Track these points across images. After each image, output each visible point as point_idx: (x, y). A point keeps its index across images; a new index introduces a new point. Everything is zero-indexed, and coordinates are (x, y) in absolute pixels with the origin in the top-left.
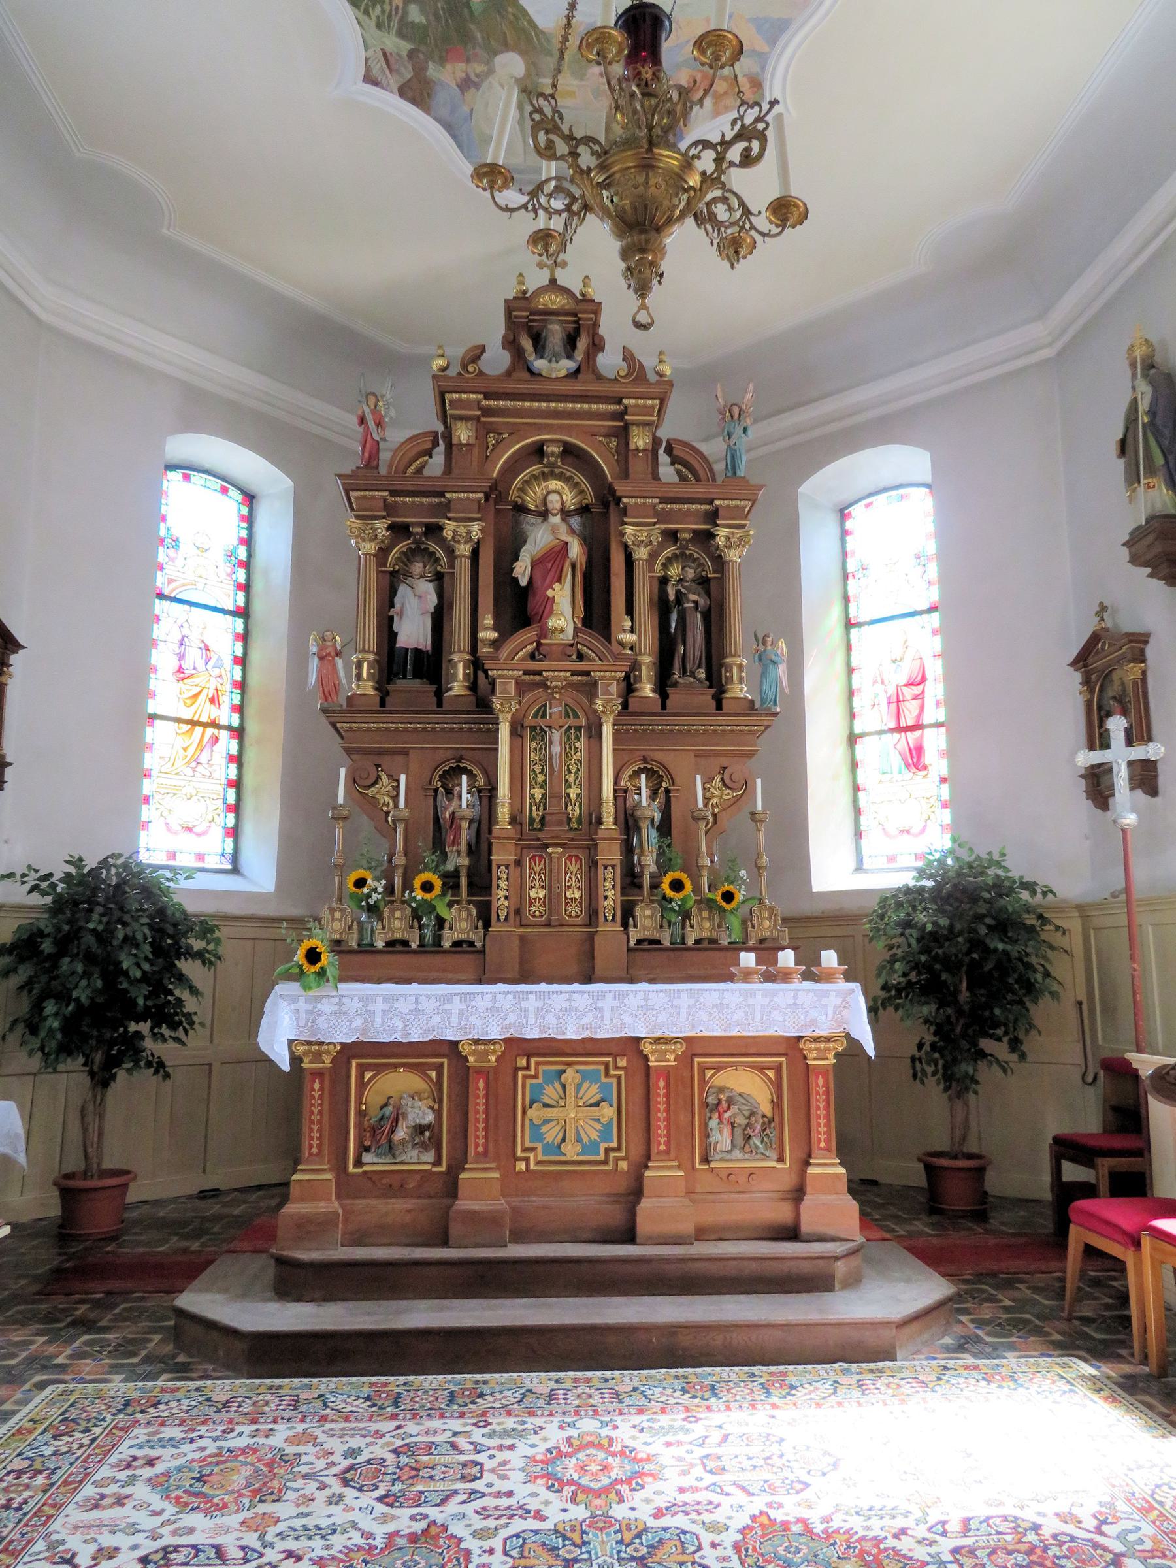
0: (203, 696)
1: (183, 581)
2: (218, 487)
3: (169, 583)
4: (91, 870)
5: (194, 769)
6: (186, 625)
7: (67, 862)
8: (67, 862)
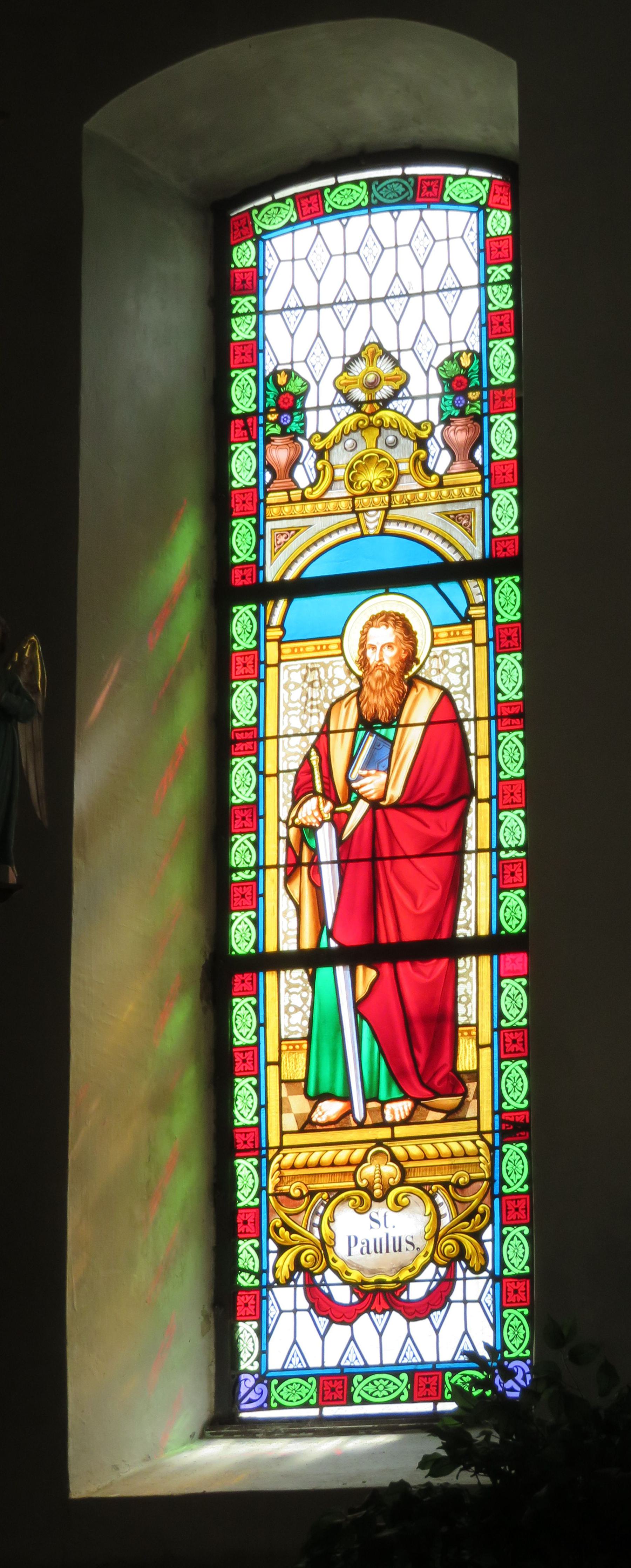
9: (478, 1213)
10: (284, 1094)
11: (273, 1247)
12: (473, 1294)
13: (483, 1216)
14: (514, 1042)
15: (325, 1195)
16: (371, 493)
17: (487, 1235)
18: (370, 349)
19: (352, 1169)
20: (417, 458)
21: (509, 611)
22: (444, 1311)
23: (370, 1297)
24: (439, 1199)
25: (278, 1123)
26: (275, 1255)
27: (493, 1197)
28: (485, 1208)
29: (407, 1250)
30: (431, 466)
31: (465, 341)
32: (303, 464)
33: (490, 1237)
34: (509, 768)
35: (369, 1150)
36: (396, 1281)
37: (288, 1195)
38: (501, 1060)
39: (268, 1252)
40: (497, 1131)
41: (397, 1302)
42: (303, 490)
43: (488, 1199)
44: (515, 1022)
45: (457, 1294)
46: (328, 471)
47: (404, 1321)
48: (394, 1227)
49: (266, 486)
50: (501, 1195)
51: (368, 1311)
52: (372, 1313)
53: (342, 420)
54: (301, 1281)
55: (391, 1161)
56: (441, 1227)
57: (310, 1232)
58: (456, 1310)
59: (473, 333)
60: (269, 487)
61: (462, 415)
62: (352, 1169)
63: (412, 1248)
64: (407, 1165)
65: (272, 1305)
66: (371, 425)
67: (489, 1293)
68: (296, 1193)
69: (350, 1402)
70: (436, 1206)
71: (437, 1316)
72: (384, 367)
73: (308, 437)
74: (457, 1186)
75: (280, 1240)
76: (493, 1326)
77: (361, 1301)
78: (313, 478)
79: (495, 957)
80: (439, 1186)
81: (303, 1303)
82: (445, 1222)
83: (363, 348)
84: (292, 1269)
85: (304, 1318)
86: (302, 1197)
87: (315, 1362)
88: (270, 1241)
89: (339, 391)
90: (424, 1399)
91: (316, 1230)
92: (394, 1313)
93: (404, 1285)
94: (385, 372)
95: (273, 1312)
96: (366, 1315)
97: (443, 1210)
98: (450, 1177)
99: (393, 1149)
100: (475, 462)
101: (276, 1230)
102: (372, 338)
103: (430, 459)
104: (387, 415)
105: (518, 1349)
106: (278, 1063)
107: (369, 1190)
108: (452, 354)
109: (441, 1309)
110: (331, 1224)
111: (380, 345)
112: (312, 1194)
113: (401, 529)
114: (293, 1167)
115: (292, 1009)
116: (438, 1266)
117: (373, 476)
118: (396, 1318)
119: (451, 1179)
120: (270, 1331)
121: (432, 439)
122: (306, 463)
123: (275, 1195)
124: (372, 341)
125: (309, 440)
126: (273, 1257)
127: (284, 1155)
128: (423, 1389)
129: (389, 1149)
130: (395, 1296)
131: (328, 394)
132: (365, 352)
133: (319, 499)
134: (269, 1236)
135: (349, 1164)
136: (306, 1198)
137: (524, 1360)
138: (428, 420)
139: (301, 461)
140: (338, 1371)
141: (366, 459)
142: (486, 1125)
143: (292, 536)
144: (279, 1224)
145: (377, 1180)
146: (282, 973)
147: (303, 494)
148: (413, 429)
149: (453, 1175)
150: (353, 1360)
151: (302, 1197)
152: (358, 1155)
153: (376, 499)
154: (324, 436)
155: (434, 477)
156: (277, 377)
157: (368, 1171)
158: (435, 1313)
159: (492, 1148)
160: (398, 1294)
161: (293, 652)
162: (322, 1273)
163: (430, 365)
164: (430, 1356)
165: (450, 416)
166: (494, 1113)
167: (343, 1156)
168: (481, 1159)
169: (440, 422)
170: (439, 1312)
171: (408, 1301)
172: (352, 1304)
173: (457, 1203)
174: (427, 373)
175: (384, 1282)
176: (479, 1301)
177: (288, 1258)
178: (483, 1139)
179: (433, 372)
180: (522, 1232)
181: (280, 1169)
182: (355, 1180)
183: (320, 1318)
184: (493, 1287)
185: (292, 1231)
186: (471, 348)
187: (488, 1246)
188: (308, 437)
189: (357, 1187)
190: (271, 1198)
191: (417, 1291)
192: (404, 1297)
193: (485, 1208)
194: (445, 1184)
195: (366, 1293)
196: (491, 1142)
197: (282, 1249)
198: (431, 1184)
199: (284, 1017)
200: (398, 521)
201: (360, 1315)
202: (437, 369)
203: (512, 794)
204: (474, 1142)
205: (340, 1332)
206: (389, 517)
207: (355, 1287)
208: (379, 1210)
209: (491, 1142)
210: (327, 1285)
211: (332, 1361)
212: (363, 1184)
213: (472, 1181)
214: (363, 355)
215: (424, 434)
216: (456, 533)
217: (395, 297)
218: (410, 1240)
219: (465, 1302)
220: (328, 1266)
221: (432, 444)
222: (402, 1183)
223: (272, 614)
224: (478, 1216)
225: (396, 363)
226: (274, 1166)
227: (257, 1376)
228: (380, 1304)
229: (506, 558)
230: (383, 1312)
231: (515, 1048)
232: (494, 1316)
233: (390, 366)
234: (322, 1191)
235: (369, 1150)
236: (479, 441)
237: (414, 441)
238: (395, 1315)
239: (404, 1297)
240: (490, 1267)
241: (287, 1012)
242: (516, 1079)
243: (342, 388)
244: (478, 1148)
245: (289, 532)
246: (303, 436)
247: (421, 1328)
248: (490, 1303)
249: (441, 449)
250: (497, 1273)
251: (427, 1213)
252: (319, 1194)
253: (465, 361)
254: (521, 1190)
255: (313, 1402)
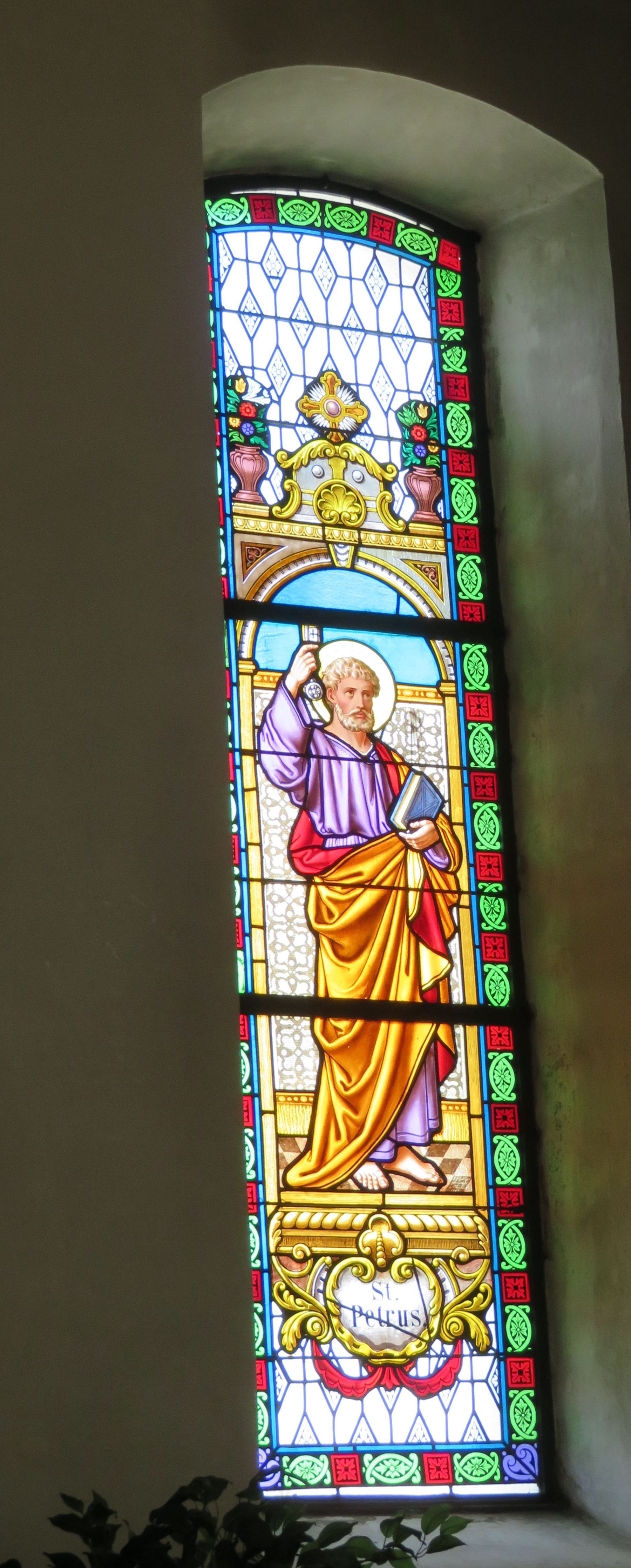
0: (391, 915)
1: (289, 547)
2: (360, 223)
3: (248, 562)
4: (134, 1541)
5: (387, 1168)
6: (311, 689)
7: (61, 1522)
8: (61, 1522)
9: (479, 1292)
10: (280, 1150)
11: (276, 1311)
12: (480, 1374)
13: (485, 1294)
14: (505, 1118)
15: (328, 1260)
16: (340, 525)
17: (490, 1316)
18: (329, 376)
19: (354, 1234)
20: (383, 498)
21: (504, 1091)
22: (453, 1389)
23: (379, 1372)
24: (442, 1274)
25: (276, 1176)
26: (281, 1319)
27: (493, 1273)
28: (484, 1287)
29: (413, 1325)
30: (396, 509)
31: (421, 392)
32: (269, 479)
33: (493, 1319)
34: (500, 1090)
35: (370, 1216)
36: (404, 1356)
37: (290, 1255)
38: (492, 1135)
39: (272, 1317)
40: (492, 1208)
41: (407, 1377)
42: (271, 507)
43: (488, 1277)
44: (508, 1181)
45: (464, 1374)
46: (296, 493)
47: (415, 1399)
48: (397, 1299)
49: (232, 495)
50: (500, 1271)
51: (378, 1386)
52: (382, 1389)
53: (307, 443)
54: (308, 1352)
55: (392, 1230)
56: (446, 1303)
57: (314, 1297)
58: (464, 1389)
59: (429, 386)
60: (235, 497)
61: (423, 465)
62: (354, 1234)
63: (418, 1323)
64: (407, 1235)
65: (279, 1375)
66: (337, 456)
67: (495, 1374)
68: (298, 1255)
69: (363, 1483)
70: (440, 1281)
71: (445, 1394)
72: (344, 397)
73: (273, 452)
74: (458, 1262)
75: (286, 1305)
76: (500, 1406)
77: (371, 1375)
78: (281, 496)
79: (482, 1028)
80: (441, 1260)
81: (313, 1374)
82: (450, 1297)
83: (322, 373)
84: (300, 1337)
85: (314, 1389)
86: (305, 1260)
87: (326, 1439)
88: (273, 1303)
89: (302, 414)
90: (438, 1482)
91: (321, 1295)
92: (404, 1389)
93: (412, 1360)
94: (346, 403)
95: (281, 1383)
96: (376, 1390)
97: (447, 1285)
98: (450, 1251)
99: (393, 1216)
100: (439, 515)
101: (280, 1293)
102: (329, 365)
103: (395, 503)
104: (354, 451)
105: (509, 1177)
106: (274, 1112)
107: (371, 1257)
108: (410, 402)
109: (450, 1387)
110: (335, 1291)
111: (337, 373)
112: (316, 1257)
113: (369, 568)
114: (295, 1227)
115: (284, 1052)
116: (444, 1342)
117: (341, 507)
118: (406, 1395)
119: (451, 1254)
120: (279, 1399)
121: (396, 484)
122: (272, 479)
123: (278, 1254)
124: (330, 368)
125: (275, 456)
126: (277, 1322)
127: (285, 1213)
128: (465, 534)
129: (388, 1216)
130: (404, 1371)
131: (290, 414)
132: (324, 378)
133: (288, 520)
134: (272, 1299)
135: (351, 1229)
136: (309, 1261)
137: (531, 1442)
138: (390, 463)
139: (268, 476)
140: (351, 1449)
141: (334, 488)
142: (482, 1201)
143: (263, 554)
144: (283, 1287)
145: (379, 1243)
146: (273, 1017)
147: (270, 510)
148: (378, 469)
149: (453, 1250)
150: (364, 1437)
151: (305, 1260)
152: (359, 1221)
153: (346, 533)
154: (290, 455)
155: (401, 522)
156: (235, 382)
157: (369, 1237)
158: (444, 1392)
159: (488, 1222)
160: (407, 1370)
161: (262, 681)
162: (329, 1342)
163: (389, 408)
164: (439, 1437)
165: (412, 465)
166: (488, 1187)
167: (345, 1218)
168: (480, 1236)
169: (404, 468)
170: (448, 1390)
171: (417, 1378)
172: (362, 1379)
173: (459, 1280)
174: (386, 414)
175: (391, 1356)
176: (486, 1381)
177: (294, 1323)
178: (480, 1215)
179: (392, 415)
180: (517, 1225)
181: (281, 1227)
182: (357, 1247)
183: (332, 1392)
184: (499, 1367)
185: (297, 1296)
186: (428, 401)
187: (492, 1327)
188: (273, 452)
189: (360, 1254)
190: (274, 1258)
191: (424, 1368)
192: (413, 1373)
193: (484, 1287)
194: (447, 1258)
195: (376, 1367)
196: (487, 1217)
197: (287, 1314)
198: (433, 1257)
199: (277, 1060)
200: (367, 561)
201: (369, 1390)
202: (396, 412)
203: (467, 538)
204: (472, 1217)
205: (350, 1406)
206: (360, 554)
207: (365, 1361)
208: (384, 1281)
209: (487, 1217)
210: (337, 1359)
211: (343, 1439)
212: (366, 1251)
213: (472, 1258)
214: (322, 381)
215: (389, 477)
216: (422, 582)
217: (351, 329)
218: (415, 1314)
219: (473, 1382)
220: (334, 1336)
221: (396, 488)
222: (404, 1254)
223: (243, 634)
224: (480, 1296)
225: (356, 397)
226: (274, 1222)
227: (268, 1451)
228: (390, 1379)
229: (472, 622)
230: (393, 1388)
231: (506, 1125)
232: (500, 1395)
233: (350, 398)
234: (325, 1255)
235: (370, 1216)
236: (441, 496)
237: (380, 481)
238: (405, 1391)
239: (413, 1373)
240: (494, 1346)
241: (279, 1054)
242: (460, 419)
243: (305, 411)
244: (477, 1225)
245: (261, 548)
246: (268, 451)
247: (430, 1406)
248: (496, 1384)
249: (405, 496)
250: (501, 1350)
251: (432, 1287)
252: (323, 1258)
253: (423, 412)
254: (514, 1183)
255: (328, 1481)
